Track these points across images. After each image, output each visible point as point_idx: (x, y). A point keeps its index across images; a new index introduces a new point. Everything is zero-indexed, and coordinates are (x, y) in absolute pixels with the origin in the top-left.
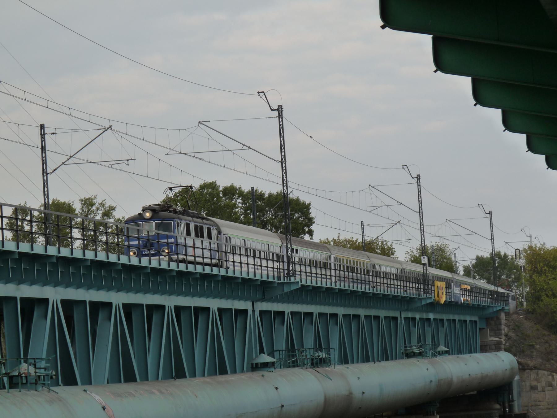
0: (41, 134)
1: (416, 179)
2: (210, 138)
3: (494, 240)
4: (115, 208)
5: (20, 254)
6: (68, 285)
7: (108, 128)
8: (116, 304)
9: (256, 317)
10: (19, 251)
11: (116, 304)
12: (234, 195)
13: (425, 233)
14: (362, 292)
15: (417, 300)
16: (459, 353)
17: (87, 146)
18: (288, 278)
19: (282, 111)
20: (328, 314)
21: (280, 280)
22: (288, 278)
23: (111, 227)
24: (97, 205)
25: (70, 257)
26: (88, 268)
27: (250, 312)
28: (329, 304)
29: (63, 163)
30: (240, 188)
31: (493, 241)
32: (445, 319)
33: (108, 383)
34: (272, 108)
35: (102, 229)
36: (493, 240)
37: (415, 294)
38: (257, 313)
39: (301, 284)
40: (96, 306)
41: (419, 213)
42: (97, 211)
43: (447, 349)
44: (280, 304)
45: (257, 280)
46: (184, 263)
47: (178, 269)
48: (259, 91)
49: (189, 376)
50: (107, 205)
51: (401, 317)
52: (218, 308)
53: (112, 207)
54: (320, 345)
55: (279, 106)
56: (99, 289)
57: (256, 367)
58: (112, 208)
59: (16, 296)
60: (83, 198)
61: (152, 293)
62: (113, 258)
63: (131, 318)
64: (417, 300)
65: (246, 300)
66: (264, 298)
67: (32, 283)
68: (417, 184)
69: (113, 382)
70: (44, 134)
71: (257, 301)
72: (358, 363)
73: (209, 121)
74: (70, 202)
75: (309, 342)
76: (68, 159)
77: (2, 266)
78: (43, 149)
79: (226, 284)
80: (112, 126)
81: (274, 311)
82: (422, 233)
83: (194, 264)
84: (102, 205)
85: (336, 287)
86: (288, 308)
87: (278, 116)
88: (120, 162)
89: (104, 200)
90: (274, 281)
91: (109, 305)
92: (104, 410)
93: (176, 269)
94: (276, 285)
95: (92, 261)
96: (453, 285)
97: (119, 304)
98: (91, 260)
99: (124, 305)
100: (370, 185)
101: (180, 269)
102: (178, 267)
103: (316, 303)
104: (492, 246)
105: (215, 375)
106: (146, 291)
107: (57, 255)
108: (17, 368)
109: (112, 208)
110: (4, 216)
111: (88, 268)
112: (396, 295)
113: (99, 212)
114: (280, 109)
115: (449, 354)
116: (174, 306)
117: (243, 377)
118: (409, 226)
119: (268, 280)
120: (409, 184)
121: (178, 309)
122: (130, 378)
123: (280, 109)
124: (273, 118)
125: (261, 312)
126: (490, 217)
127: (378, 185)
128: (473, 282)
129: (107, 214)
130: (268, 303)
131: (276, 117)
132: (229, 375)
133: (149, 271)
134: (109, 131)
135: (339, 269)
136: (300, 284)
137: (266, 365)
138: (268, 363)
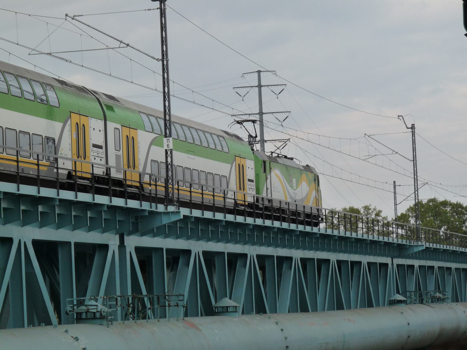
0: (394, 186)
3: (417, 162)
4: (382, 211)
5: (226, 222)
6: (261, 245)
7: (426, 183)
8: (295, 258)
10: (226, 220)
11: (295, 258)
12: (447, 205)
13: (418, 181)
14: (434, 248)
16: (441, 300)
18: (417, 242)
20: (406, 265)
21: (411, 244)
22: (417, 242)
23: (380, 222)
24: (372, 210)
25: (295, 230)
26: (298, 236)
27: (390, 265)
28: (445, 261)
29: (404, 200)
30: (450, 201)
31: (416, 162)
32: (225, 252)
33: (289, 312)
34: (408, 127)
35: (375, 223)
36: (415, 162)
38: (395, 266)
39: (426, 246)
40: (281, 260)
41: (413, 162)
42: (372, 213)
43: (406, 299)
44: (431, 261)
45: (394, 243)
46: (243, 216)
47: (339, 235)
48: (399, 115)
49: (359, 307)
50: (377, 210)
51: (392, 264)
52: (367, 262)
53: (380, 210)
54: (439, 289)
56: (297, 249)
57: (393, 303)
58: (380, 211)
59: (451, 267)
60: (364, 206)
61: (243, 243)
62: (381, 239)
63: (321, 269)
65: (387, 256)
66: (400, 256)
67: (237, 242)
68: (411, 133)
69: (293, 312)
70: (395, 186)
71: (395, 258)
72: (465, 301)
74: (359, 209)
75: (431, 286)
76: (407, 198)
77: (32, 210)
78: (395, 193)
79: (457, 256)
81: (428, 266)
82: (416, 181)
83: (280, 221)
84: (374, 209)
85: (191, 215)
86: (416, 263)
89: (376, 207)
90: (407, 244)
91: (290, 259)
92: (282, 331)
93: (252, 224)
94: (408, 247)
95: (278, 228)
97: (297, 258)
98: (277, 227)
99: (301, 259)
100: (365, 134)
101: (340, 235)
102: (255, 222)
103: (436, 260)
104: (416, 170)
105: (276, 313)
106: (317, 249)
107: (253, 224)
108: (436, 294)
109: (380, 211)
110: (59, 168)
111: (298, 236)
112: (435, 248)
113: (373, 213)
114: (413, 127)
115: (406, 304)
116: (203, 251)
117: (246, 319)
119: (402, 243)
120: (403, 133)
121: (340, 263)
122: (304, 309)
124: (153, 9)
125: (398, 266)
126: (412, 132)
127: (374, 134)
129: (378, 215)
130: (410, 260)
131: (410, 132)
132: (56, 326)
133: (318, 236)
134: (426, 185)
135: (124, 178)
136: (425, 246)
137: (400, 302)
138: (401, 300)
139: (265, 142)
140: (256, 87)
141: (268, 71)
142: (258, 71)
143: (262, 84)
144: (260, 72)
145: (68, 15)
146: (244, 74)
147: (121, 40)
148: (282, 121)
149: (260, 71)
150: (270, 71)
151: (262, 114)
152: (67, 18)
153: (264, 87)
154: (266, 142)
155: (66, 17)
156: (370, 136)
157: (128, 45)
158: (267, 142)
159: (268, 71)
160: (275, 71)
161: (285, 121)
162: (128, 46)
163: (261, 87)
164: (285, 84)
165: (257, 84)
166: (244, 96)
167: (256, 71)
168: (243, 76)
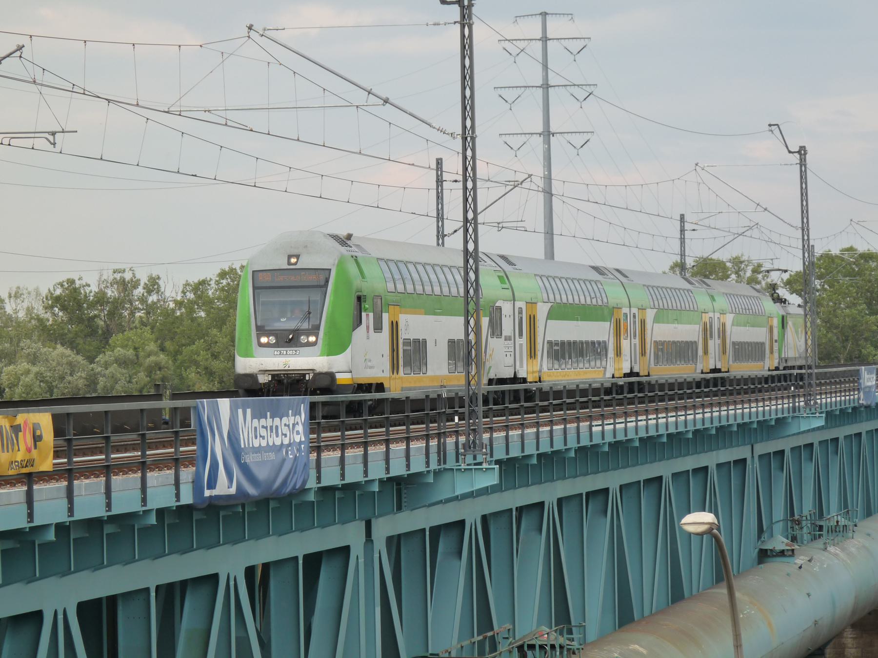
1: (797, 155)
2: (271, 60)
9: (376, 556)
15: (430, 479)
17: (488, 205)
19: (805, 154)
37: (834, 404)
38: (380, 544)
49: (320, 487)
55: (801, 147)
64: (790, 420)
73: (284, 29)
80: (23, 46)
83: (580, 390)
87: (459, 20)
88: (37, 135)
96: (863, 371)
114: (802, 152)
118: (790, 246)
123: (803, 152)
128: (473, 358)
131: (455, 23)
139: (551, 135)
140: (538, 40)
141: (575, 85)
142: (542, 13)
143: (549, 36)
144: (546, 15)
145: (253, 28)
146: (517, 17)
147: (369, 89)
148: (575, 54)
149: (545, 13)
150: (578, 85)
151: (548, 88)
152: (852, 223)
153: (552, 40)
154: (553, 136)
155: (249, 32)
156: (267, 33)
157: (386, 101)
158: (555, 135)
159: (575, 85)
160: (571, 14)
161: (587, 99)
162: (386, 102)
163: (546, 41)
164: (595, 84)
165: (539, 36)
166: (518, 55)
167: (539, 13)
168: (516, 20)
